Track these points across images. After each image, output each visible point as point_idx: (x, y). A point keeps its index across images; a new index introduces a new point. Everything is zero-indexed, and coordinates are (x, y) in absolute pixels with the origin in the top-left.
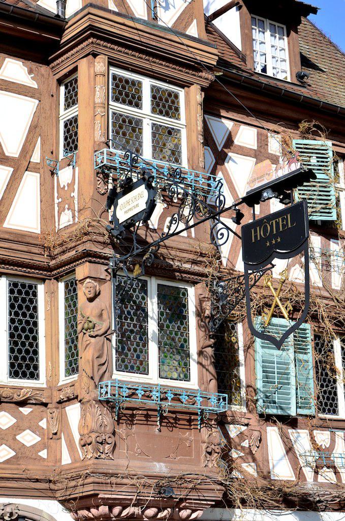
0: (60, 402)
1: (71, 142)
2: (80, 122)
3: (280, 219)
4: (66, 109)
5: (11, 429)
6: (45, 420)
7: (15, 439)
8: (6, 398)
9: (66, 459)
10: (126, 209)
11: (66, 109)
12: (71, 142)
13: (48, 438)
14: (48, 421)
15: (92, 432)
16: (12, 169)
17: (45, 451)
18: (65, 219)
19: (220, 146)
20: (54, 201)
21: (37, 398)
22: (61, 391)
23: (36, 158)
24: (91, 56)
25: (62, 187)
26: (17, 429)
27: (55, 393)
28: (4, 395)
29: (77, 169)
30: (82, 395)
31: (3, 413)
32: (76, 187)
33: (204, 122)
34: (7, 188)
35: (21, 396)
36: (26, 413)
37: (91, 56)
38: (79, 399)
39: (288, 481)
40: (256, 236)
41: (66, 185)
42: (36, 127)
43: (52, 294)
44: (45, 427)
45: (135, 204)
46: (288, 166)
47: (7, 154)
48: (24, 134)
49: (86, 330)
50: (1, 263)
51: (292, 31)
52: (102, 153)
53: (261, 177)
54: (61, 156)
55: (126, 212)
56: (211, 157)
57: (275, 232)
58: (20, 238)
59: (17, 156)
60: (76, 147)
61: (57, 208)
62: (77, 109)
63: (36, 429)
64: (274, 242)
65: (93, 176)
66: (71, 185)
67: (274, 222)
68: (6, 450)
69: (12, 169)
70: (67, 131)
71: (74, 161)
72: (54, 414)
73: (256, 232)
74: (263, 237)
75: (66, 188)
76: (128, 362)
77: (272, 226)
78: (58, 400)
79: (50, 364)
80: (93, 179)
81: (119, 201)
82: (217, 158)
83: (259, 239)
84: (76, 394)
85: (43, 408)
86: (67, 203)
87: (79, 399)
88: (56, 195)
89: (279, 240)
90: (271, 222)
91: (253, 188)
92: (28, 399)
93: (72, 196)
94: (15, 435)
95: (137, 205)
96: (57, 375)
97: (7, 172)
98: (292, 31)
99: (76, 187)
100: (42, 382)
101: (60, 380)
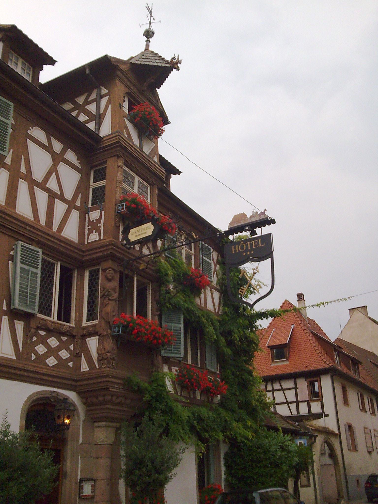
3: (253, 242)
4: (93, 183)
9: (85, 367)
10: (136, 235)
11: (93, 183)
13: (74, 356)
14: (74, 345)
15: (108, 352)
17: (72, 363)
18: (94, 237)
24: (116, 157)
25: (91, 220)
26: (59, 348)
29: (103, 212)
30: (101, 331)
37: (116, 157)
38: (99, 334)
40: (235, 251)
41: (95, 220)
42: (79, 188)
43: (81, 277)
44: (72, 349)
45: (145, 231)
52: (123, 205)
54: (90, 206)
55: (136, 236)
57: (249, 248)
58: (68, 242)
60: (104, 201)
62: (105, 182)
63: (68, 350)
66: (99, 221)
67: (249, 243)
68: (53, 360)
73: (235, 248)
74: (240, 250)
78: (82, 334)
79: (78, 314)
81: (131, 230)
83: (237, 251)
87: (99, 334)
88: (87, 224)
90: (246, 243)
95: (145, 233)
96: (81, 320)
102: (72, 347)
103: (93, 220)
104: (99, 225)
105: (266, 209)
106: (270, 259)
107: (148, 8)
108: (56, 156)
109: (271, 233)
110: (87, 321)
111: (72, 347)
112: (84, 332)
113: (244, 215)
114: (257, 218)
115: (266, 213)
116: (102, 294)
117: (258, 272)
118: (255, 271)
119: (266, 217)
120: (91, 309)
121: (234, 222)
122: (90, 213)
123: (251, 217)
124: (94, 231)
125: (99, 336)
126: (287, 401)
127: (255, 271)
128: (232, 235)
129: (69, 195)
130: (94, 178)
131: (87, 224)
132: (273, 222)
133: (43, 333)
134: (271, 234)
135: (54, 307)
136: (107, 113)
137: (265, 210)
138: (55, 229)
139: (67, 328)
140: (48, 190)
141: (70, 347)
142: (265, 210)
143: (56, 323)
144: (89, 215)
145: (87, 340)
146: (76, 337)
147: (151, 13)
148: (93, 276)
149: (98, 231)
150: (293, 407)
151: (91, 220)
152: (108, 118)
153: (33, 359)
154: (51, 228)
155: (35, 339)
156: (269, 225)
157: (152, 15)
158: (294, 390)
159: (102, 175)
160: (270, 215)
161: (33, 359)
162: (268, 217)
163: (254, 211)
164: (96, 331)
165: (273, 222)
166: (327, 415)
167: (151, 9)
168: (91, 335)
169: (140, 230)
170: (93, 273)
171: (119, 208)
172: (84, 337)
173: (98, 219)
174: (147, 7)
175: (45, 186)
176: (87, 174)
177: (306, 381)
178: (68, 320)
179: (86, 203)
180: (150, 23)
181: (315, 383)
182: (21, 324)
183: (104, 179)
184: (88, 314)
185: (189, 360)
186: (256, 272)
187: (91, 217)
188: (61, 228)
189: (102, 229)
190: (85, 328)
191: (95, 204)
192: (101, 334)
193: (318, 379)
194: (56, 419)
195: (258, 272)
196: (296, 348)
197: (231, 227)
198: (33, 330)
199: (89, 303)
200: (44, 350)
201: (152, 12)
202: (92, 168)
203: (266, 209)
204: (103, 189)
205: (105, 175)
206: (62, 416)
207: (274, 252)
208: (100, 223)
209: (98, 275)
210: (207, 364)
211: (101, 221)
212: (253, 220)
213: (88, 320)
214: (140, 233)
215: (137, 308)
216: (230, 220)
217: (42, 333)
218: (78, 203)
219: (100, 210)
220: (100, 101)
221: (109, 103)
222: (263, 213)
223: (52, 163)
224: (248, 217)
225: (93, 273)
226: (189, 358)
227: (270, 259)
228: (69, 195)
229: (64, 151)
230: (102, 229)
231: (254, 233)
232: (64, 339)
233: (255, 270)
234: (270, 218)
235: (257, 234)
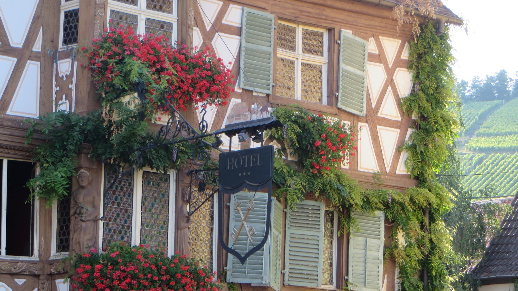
1: (70, 33)
8: (4, 270)
12: (70, 33)
16: (16, 60)
19: (208, 26)
20: (52, 88)
21: (31, 270)
22: (52, 266)
23: (37, 47)
25: (60, 76)
27: (47, 266)
28: (3, 268)
29: (76, 63)
31: (1, 283)
34: (11, 77)
35: (17, 269)
36: (20, 284)
39: (281, 47)
41: (64, 76)
46: (261, 112)
47: (12, 45)
48: (24, 34)
50: (2, 147)
53: (240, 115)
56: (199, 38)
59: (20, 46)
61: (55, 96)
64: (245, 174)
66: (69, 77)
69: (16, 60)
70: (67, 22)
71: (74, 55)
72: (45, 285)
75: (65, 79)
76: (151, 4)
77: (244, 160)
78: (49, 273)
79: (43, 239)
82: (205, 38)
84: (66, 270)
85: (36, 279)
86: (64, 91)
88: (54, 82)
89: (249, 173)
92: (24, 271)
97: (12, 62)
100: (35, 257)
101: (52, 255)
112: (52, 270)
122: (59, 62)
124: (64, 96)
131: (54, 82)
135: (135, 231)
139: (23, 266)
144: (56, 64)
146: (41, 277)
151: (60, 76)
168: (60, 275)
172: (52, 277)
173: (68, 74)
179: (54, 41)
184: (65, 22)
185: (15, 258)
190: (51, 263)
200: (219, 4)
210: (340, 99)
215: (227, 9)
226: (19, 258)
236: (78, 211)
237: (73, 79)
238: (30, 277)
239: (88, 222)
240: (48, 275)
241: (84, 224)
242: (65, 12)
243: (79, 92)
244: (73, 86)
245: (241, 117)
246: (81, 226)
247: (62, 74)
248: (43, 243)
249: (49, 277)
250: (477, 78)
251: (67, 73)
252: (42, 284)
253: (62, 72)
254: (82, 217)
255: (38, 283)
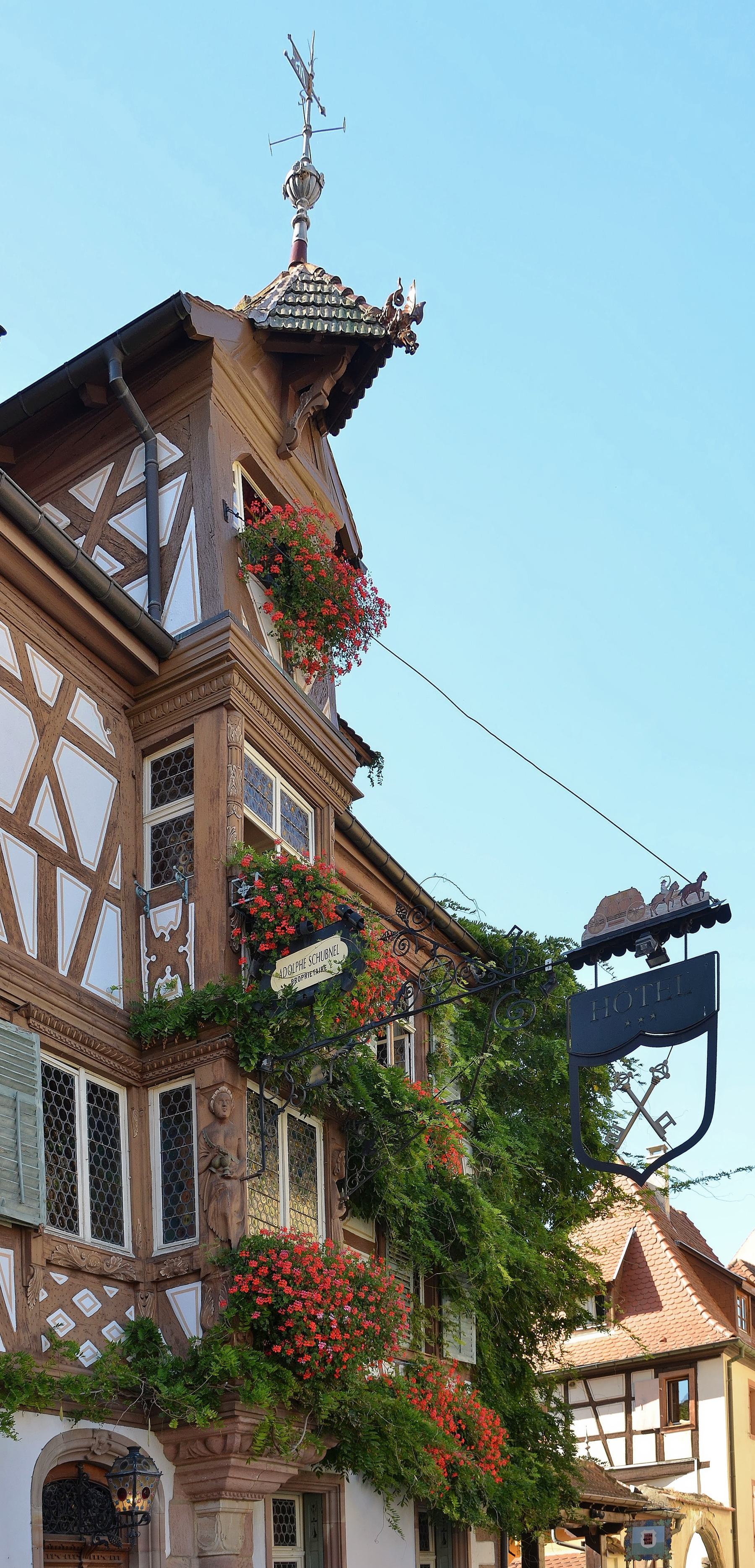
0: (156, 1282)
2: (197, 825)
5: (95, 1318)
6: (132, 1308)
7: (100, 1333)
25: (157, 935)
29: (192, 906)
32: (190, 936)
33: (664, 1139)
38: (202, 1275)
41: (167, 933)
46: (680, 897)
49: (216, 1168)
51: (707, 1033)
53: (620, 914)
54: (147, 886)
61: (148, 972)
65: (224, 918)
66: (179, 935)
75: (167, 938)
78: (155, 1278)
80: (224, 924)
87: (202, 1275)
91: (597, 935)
93: (180, 951)
94: (101, 1328)
98: (707, 1033)
99: (190, 936)
101: (155, 1249)
102: (131, 1313)
103: (163, 935)
104: (181, 949)
105: (704, 873)
106: (705, 1035)
107: (295, 59)
108: (45, 716)
109: (716, 952)
110: (165, 1242)
111: (131, 1314)
112: (161, 1272)
113: (633, 895)
114: (676, 905)
115: (705, 885)
116: (205, 1163)
117: (667, 1076)
118: (656, 1074)
119: (703, 900)
120: (174, 1207)
121: (602, 921)
122: (152, 911)
123: (655, 901)
124: (168, 969)
125: (203, 1280)
126: (637, 1433)
127: (656, 1074)
128: (589, 964)
129: (89, 856)
130: (155, 790)
132: (723, 914)
133: (61, 1278)
134: (716, 955)
136: (184, 545)
137: (703, 877)
138: (63, 970)
140: (34, 839)
141: (127, 1313)
142: (703, 877)
143: (89, 1249)
144: (148, 920)
145: (169, 1292)
146: (141, 1287)
147: (308, 81)
148: (172, 1110)
149: (179, 969)
150: (617, 1447)
151: (157, 935)
152: (187, 559)
153: (44, 1349)
154: (53, 964)
155: (43, 1295)
156: (709, 925)
157: (315, 89)
158: (623, 1403)
159: (179, 780)
160: (714, 889)
161: (44, 1349)
162: (710, 898)
163: (667, 879)
164: (195, 1267)
165: (723, 914)
166: (707, 1465)
167: (306, 60)
168: (178, 1279)
169: (307, 961)
170: (172, 1102)
171: (239, 891)
172: (160, 1284)
173: (175, 928)
174: (291, 56)
175: (27, 827)
176: (134, 777)
177: (658, 1379)
178: (118, 1239)
180: (309, 132)
181: (680, 1383)
182: (8, 1256)
183: (188, 790)
186: (661, 1076)
187: (156, 924)
188: (78, 968)
189: (190, 962)
190: (159, 1261)
191: (173, 1145)
192: (208, 1275)
193: (691, 1372)
194: (115, 1499)
195: (667, 1076)
196: (645, 1291)
197: (590, 936)
198: (39, 1273)
199: (167, 1190)
201: (312, 76)
202: (145, 753)
203: (704, 873)
204: (184, 824)
205: (191, 776)
206: (129, 1491)
207: (719, 1013)
208: (184, 946)
209: (185, 1106)
211: (187, 936)
212: (662, 910)
213: (169, 1237)
214: (308, 969)
216: (588, 913)
217: (60, 1279)
218: (115, 880)
219: (180, 901)
220: (157, 495)
221: (189, 500)
222: (695, 887)
223: (38, 743)
224: (648, 901)
225: (172, 1102)
227: (705, 1035)
228: (89, 856)
229: (65, 694)
230: (190, 962)
231: (658, 955)
232: (111, 1291)
233: (658, 1071)
234: (716, 901)
235: (668, 960)
236: (217, 1161)
237: (146, 949)
238: (123, 1286)
239: (234, 1181)
240: (153, 1282)
241: (228, 1184)
242: (153, 828)
243: (203, 956)
244: (189, 948)
245: (625, 918)
246: (225, 1186)
247: (162, 931)
248: (140, 1228)
249: (154, 1287)
250: (666, 1120)
251: (172, 927)
252: (142, 1298)
253: (162, 927)
254: (224, 1171)
255: (136, 1297)
